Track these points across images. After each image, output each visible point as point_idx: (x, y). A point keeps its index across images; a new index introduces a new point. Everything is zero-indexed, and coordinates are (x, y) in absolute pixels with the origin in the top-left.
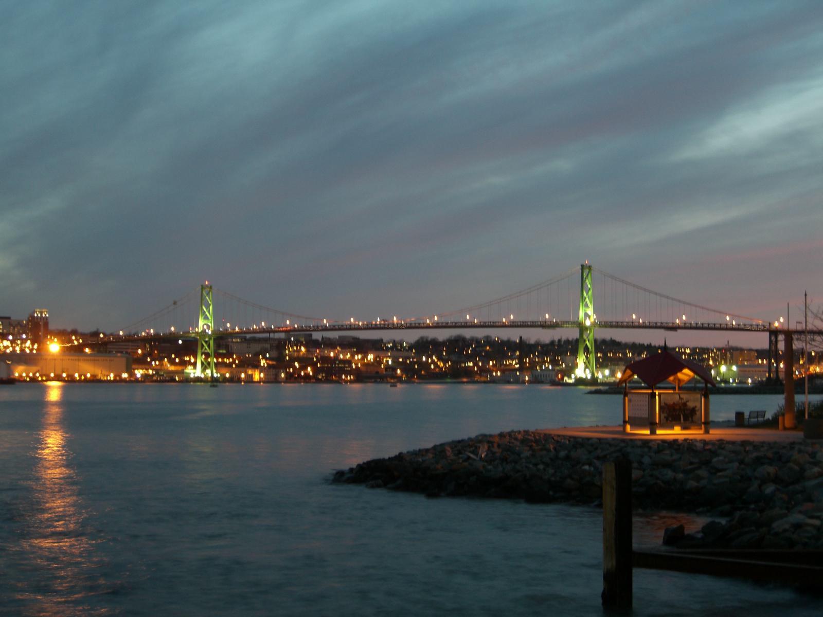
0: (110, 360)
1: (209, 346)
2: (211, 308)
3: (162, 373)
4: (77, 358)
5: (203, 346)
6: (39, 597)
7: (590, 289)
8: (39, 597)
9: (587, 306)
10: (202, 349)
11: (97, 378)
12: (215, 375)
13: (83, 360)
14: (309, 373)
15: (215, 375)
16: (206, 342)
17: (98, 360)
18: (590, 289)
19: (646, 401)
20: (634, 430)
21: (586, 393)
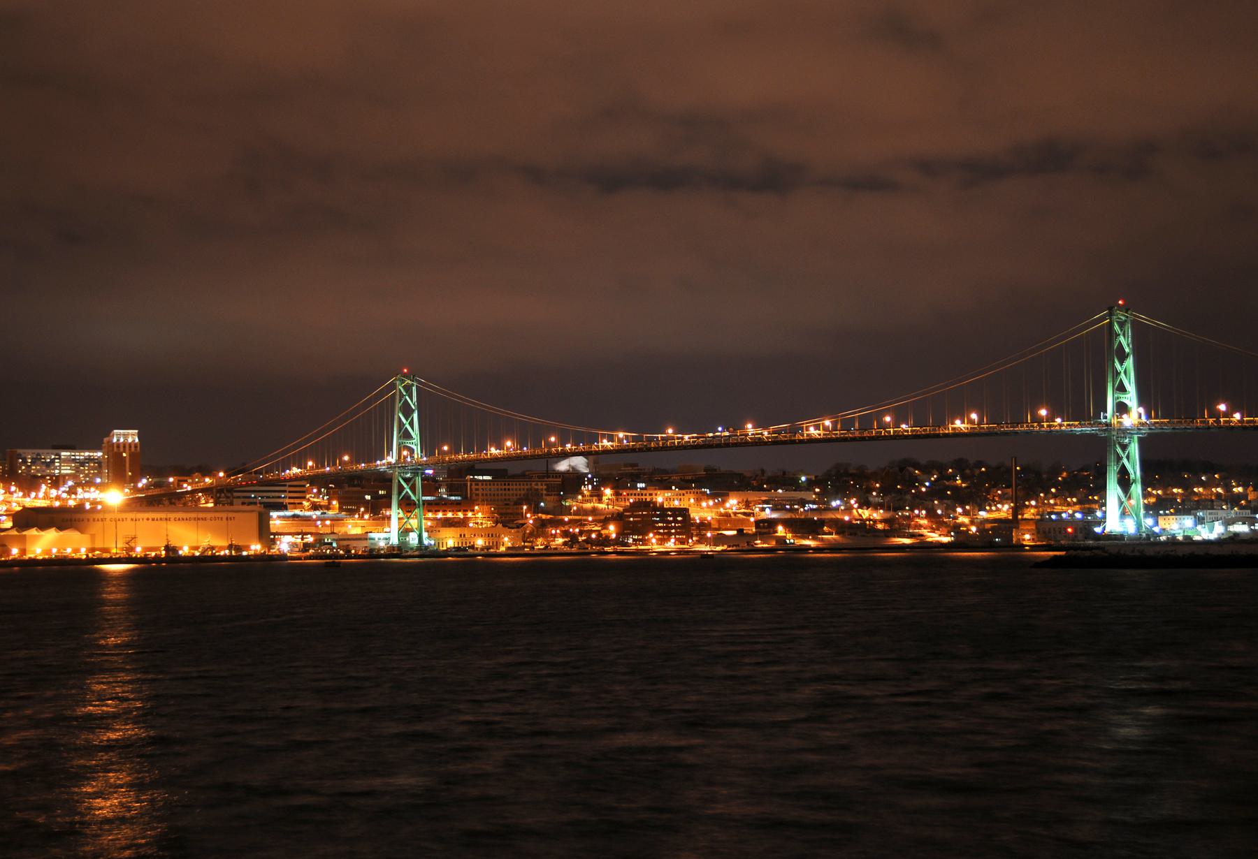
0: (227, 519)
1: (413, 489)
2: (415, 416)
3: (330, 541)
4: (163, 515)
5: (401, 488)
6: (1091, 542)
7: (1128, 354)
8: (1091, 542)
9: (1122, 388)
10: (400, 493)
11: (181, 552)
12: (426, 542)
13: (114, 512)
14: (611, 534)
15: (426, 542)
16: (407, 480)
17: (205, 519)
18: (1128, 354)
19: (93, 550)
20: (992, 556)
21: (1031, 567)
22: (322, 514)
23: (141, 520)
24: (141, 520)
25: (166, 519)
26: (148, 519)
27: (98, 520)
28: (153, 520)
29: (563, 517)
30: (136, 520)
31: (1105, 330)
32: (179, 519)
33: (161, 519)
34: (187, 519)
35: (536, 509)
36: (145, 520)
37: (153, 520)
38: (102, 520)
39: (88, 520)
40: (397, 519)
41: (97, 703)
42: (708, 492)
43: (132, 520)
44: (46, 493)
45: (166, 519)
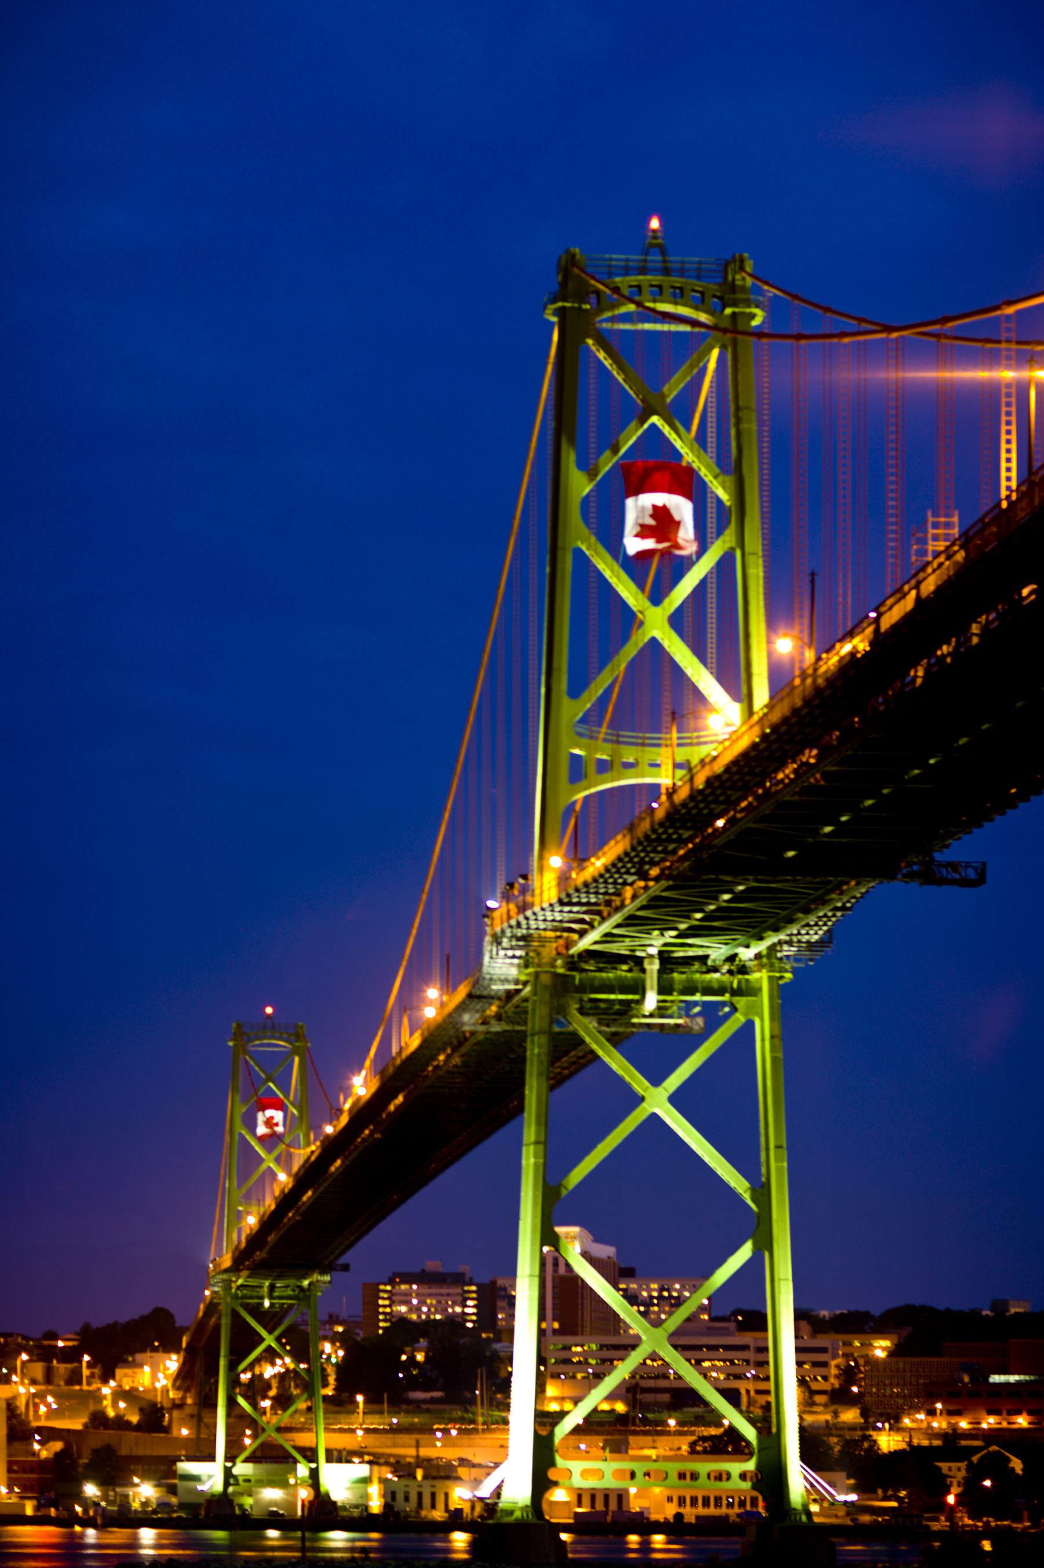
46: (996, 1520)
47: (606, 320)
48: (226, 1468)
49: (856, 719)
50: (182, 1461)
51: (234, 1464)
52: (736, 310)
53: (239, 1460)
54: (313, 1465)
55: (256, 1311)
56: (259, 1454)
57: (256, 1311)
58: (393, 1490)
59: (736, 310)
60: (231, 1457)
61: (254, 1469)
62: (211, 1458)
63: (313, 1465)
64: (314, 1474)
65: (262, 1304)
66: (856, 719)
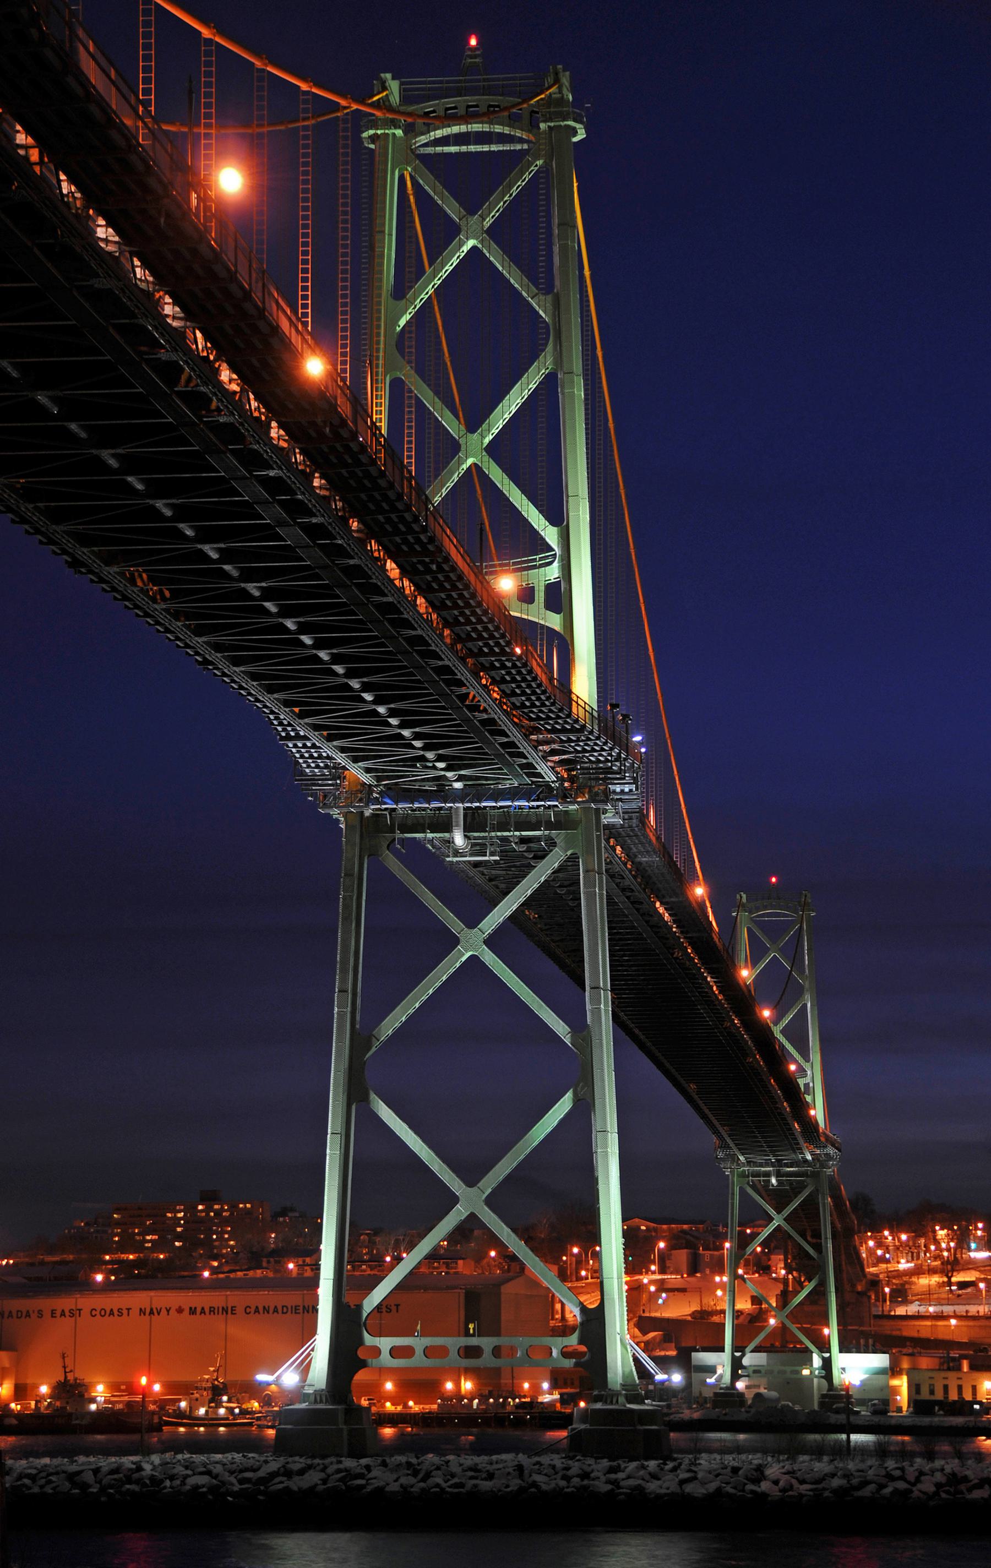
22: (244, 1275)
23: (164, 1312)
24: (164, 1312)
25: (225, 1310)
26: (180, 1310)
27: (63, 1314)
28: (193, 1311)
29: (641, 1277)
30: (151, 1312)
31: (278, 128)
32: (257, 1310)
33: (212, 1310)
34: (276, 1310)
35: (834, 1418)
36: (172, 1312)
37: (193, 1311)
38: (72, 1314)
39: (40, 1314)
40: (936, 1393)
41: (330, 782)
42: (388, 1404)
43: (142, 1311)
44: (125, 251)
45: (225, 1310)
46: (788, 1405)
47: (521, 141)
48: (733, 1357)
49: (273, 1236)
50: (698, 1351)
51: (743, 1355)
52: (552, 124)
53: (748, 1350)
54: (827, 1355)
55: (765, 1191)
56: (761, 1346)
57: (765, 1191)
58: (917, 1383)
59: (552, 124)
60: (739, 1347)
61: (768, 1359)
62: (722, 1350)
63: (827, 1355)
64: (827, 1364)
65: (769, 1181)
66: (273, 1236)
